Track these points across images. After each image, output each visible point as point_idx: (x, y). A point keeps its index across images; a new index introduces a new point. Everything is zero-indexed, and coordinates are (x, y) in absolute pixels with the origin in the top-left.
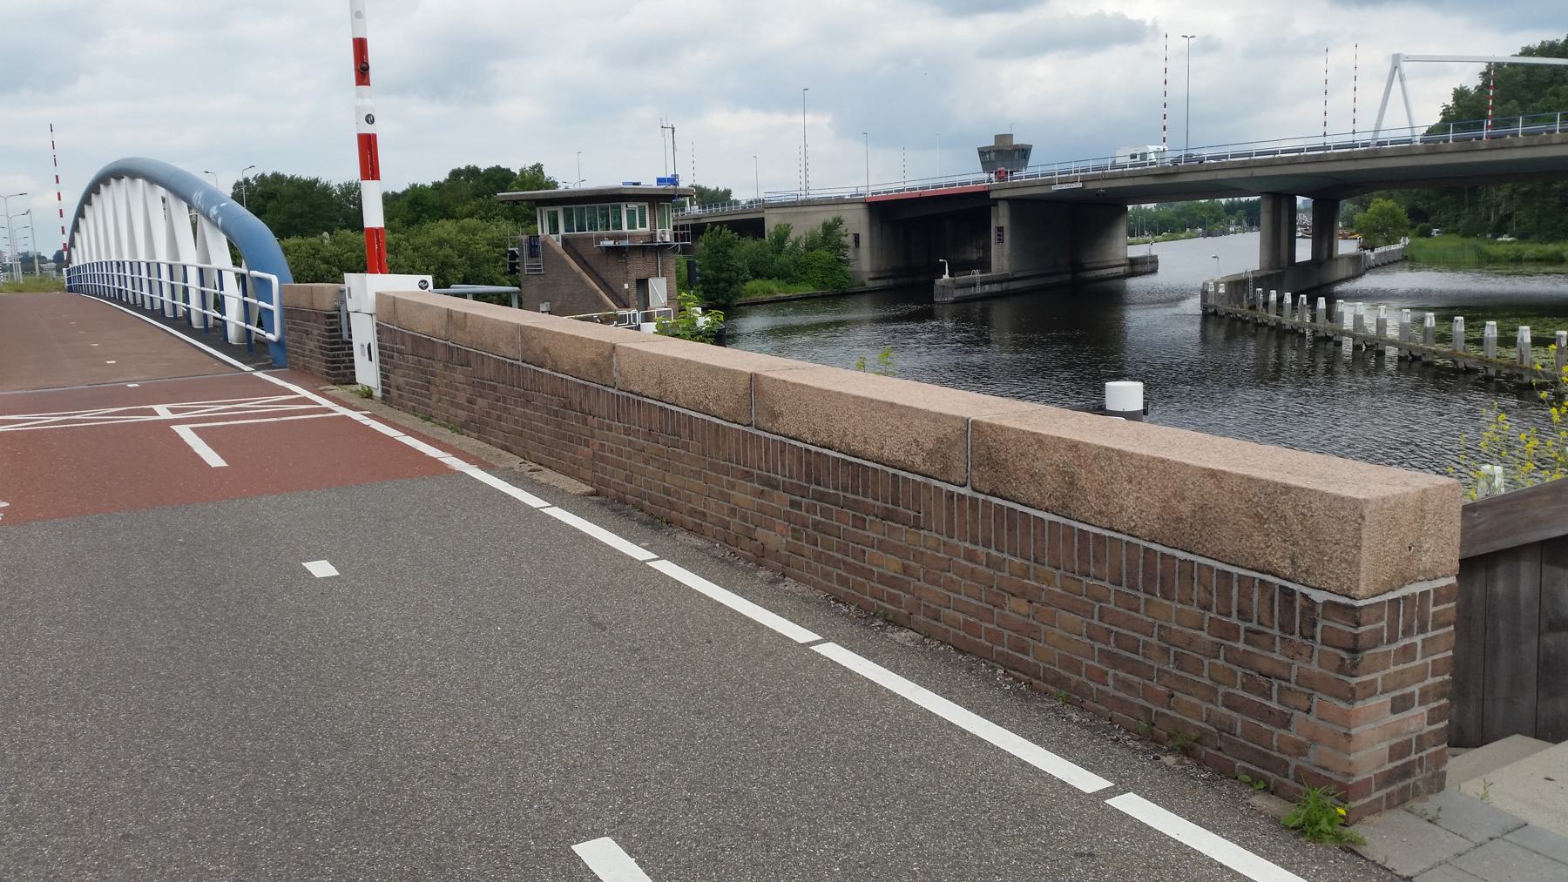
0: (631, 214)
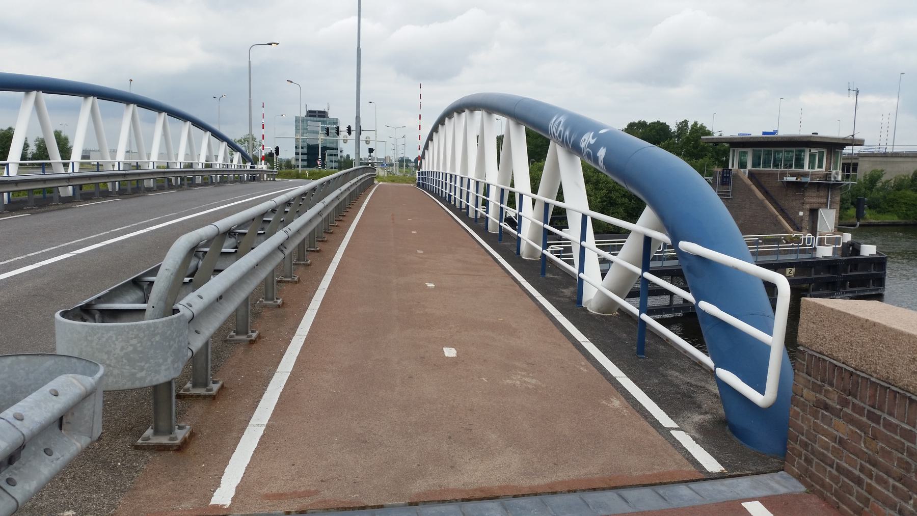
0: (812, 157)
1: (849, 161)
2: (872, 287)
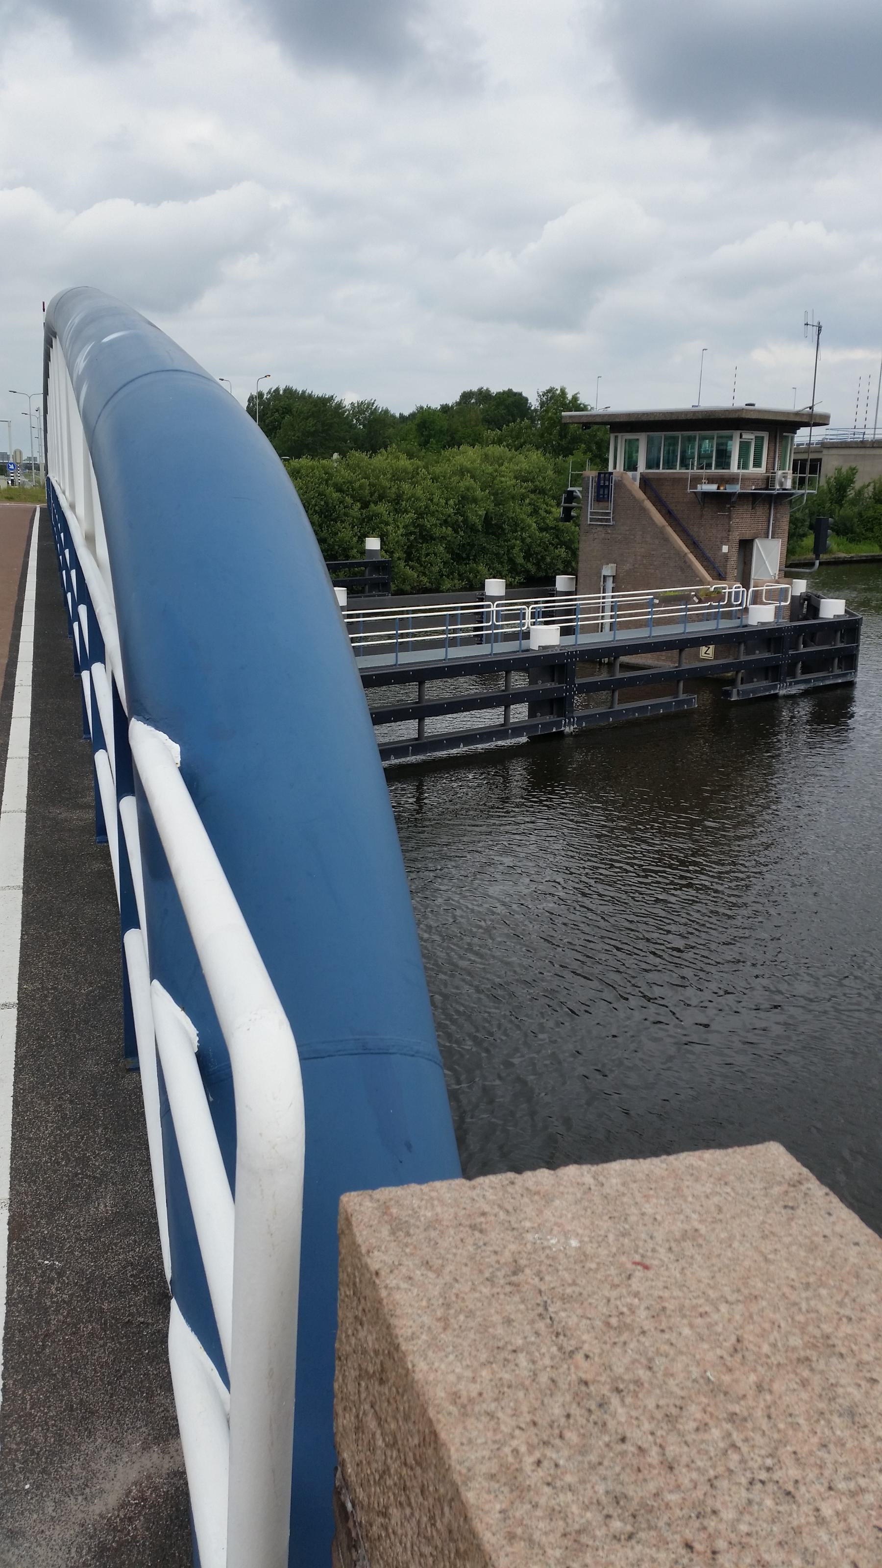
0: (744, 447)
1: (803, 456)
2: (837, 671)
